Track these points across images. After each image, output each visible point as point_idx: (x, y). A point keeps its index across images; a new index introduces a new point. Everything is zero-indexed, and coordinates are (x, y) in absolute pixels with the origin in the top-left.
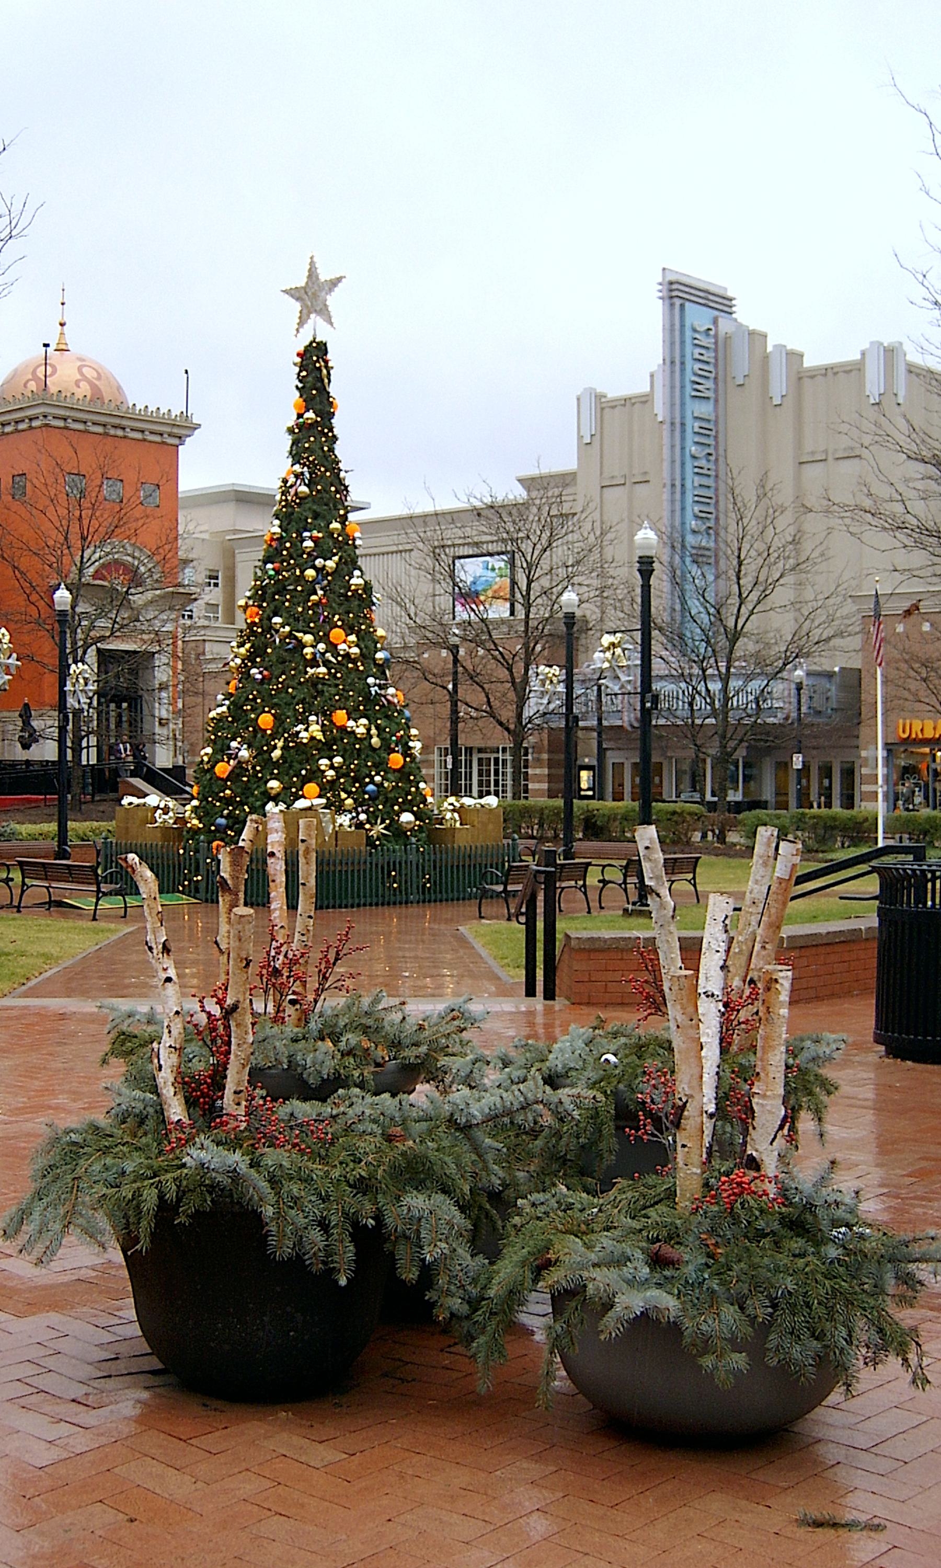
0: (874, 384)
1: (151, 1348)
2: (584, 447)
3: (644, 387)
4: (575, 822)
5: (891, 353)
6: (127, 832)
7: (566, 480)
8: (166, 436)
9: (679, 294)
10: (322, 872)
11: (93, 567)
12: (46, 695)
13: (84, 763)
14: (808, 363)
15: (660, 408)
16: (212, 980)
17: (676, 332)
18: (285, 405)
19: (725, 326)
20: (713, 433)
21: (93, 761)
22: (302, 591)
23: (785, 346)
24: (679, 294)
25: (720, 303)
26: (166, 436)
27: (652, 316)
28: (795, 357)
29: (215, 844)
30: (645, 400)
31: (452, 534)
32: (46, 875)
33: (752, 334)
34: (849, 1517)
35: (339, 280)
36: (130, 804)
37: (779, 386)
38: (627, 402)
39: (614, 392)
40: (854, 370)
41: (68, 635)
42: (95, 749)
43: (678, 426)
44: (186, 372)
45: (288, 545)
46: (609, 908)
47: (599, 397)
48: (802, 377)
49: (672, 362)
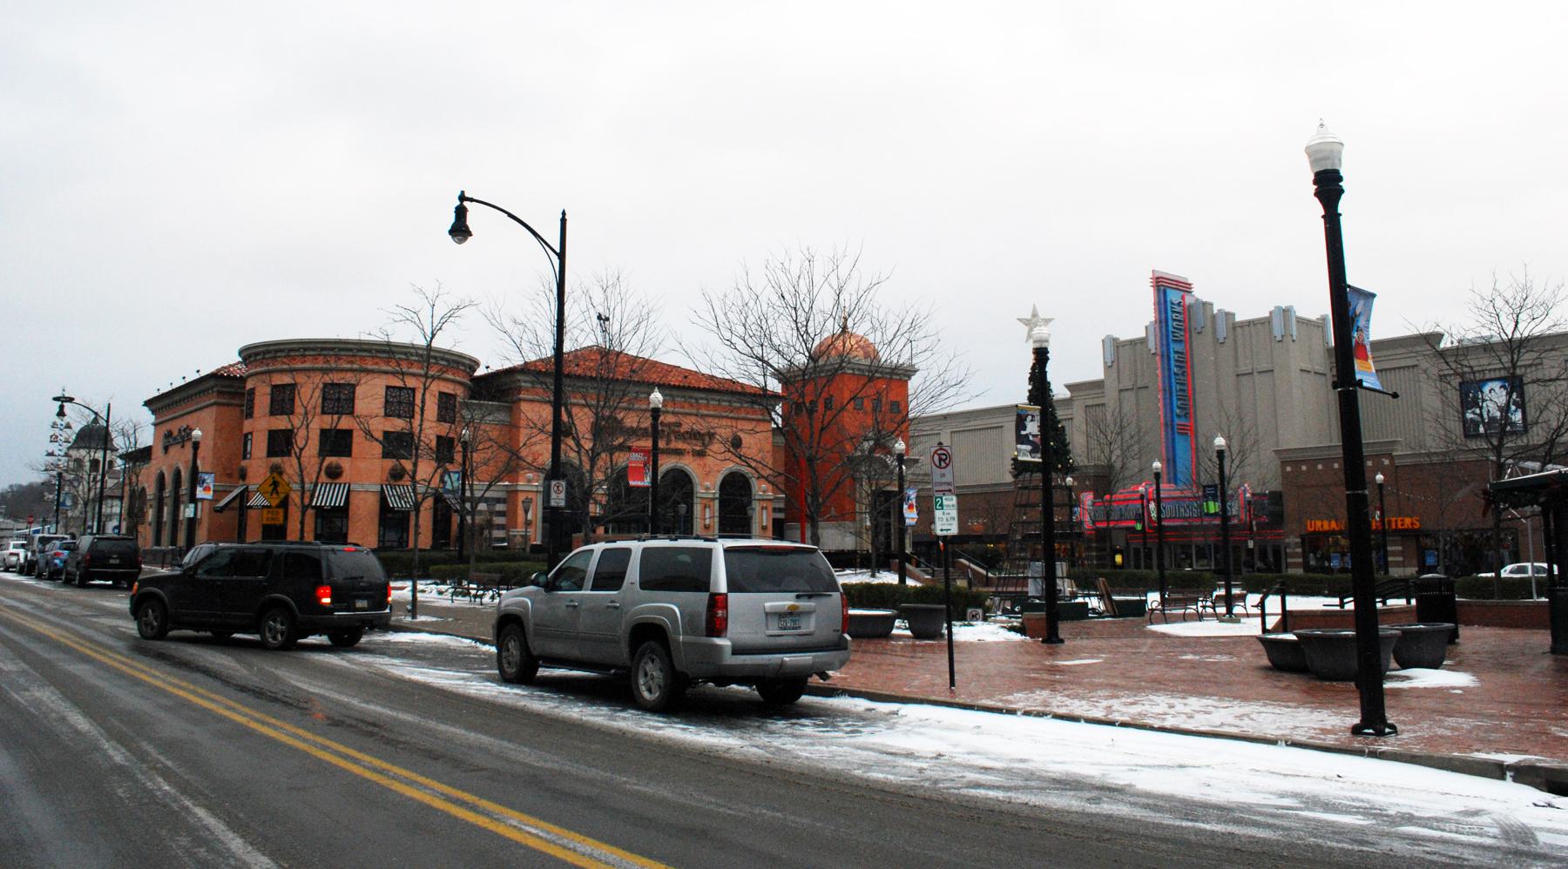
0: (1278, 331)
1: (576, 354)
2: (1108, 368)
3: (1143, 335)
4: (154, 503)
5: (1286, 312)
6: (1108, 515)
7: (1096, 385)
8: (901, 374)
9: (1163, 286)
10: (1481, 741)
11: (581, 848)
12: (511, 746)
13: (392, 584)
14: (1238, 319)
15: (1152, 345)
16: (1244, 557)
17: (1162, 304)
18: (1030, 360)
19: (1189, 300)
20: (165, 546)
21: (895, 632)
22: (1114, 565)
23: (1432, 339)
24: (1163, 286)
25: (1185, 287)
26: (901, 374)
27: (1148, 296)
28: (1229, 316)
29: (77, 513)
30: (1143, 341)
31: (1479, 362)
32: (1229, 611)
33: (1204, 304)
34: (1317, 304)
35: (564, 213)
36: (650, 690)
37: (1222, 332)
38: (1133, 343)
39: (1124, 336)
40: (1265, 323)
41: (1225, 658)
42: (1289, 599)
43: (1166, 357)
44: (1328, 186)
45: (1118, 559)
46: (1238, 390)
47: (1115, 340)
48: (1238, 328)
49: (374, 725)
